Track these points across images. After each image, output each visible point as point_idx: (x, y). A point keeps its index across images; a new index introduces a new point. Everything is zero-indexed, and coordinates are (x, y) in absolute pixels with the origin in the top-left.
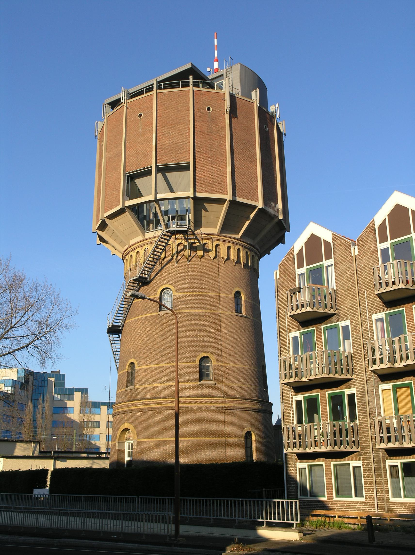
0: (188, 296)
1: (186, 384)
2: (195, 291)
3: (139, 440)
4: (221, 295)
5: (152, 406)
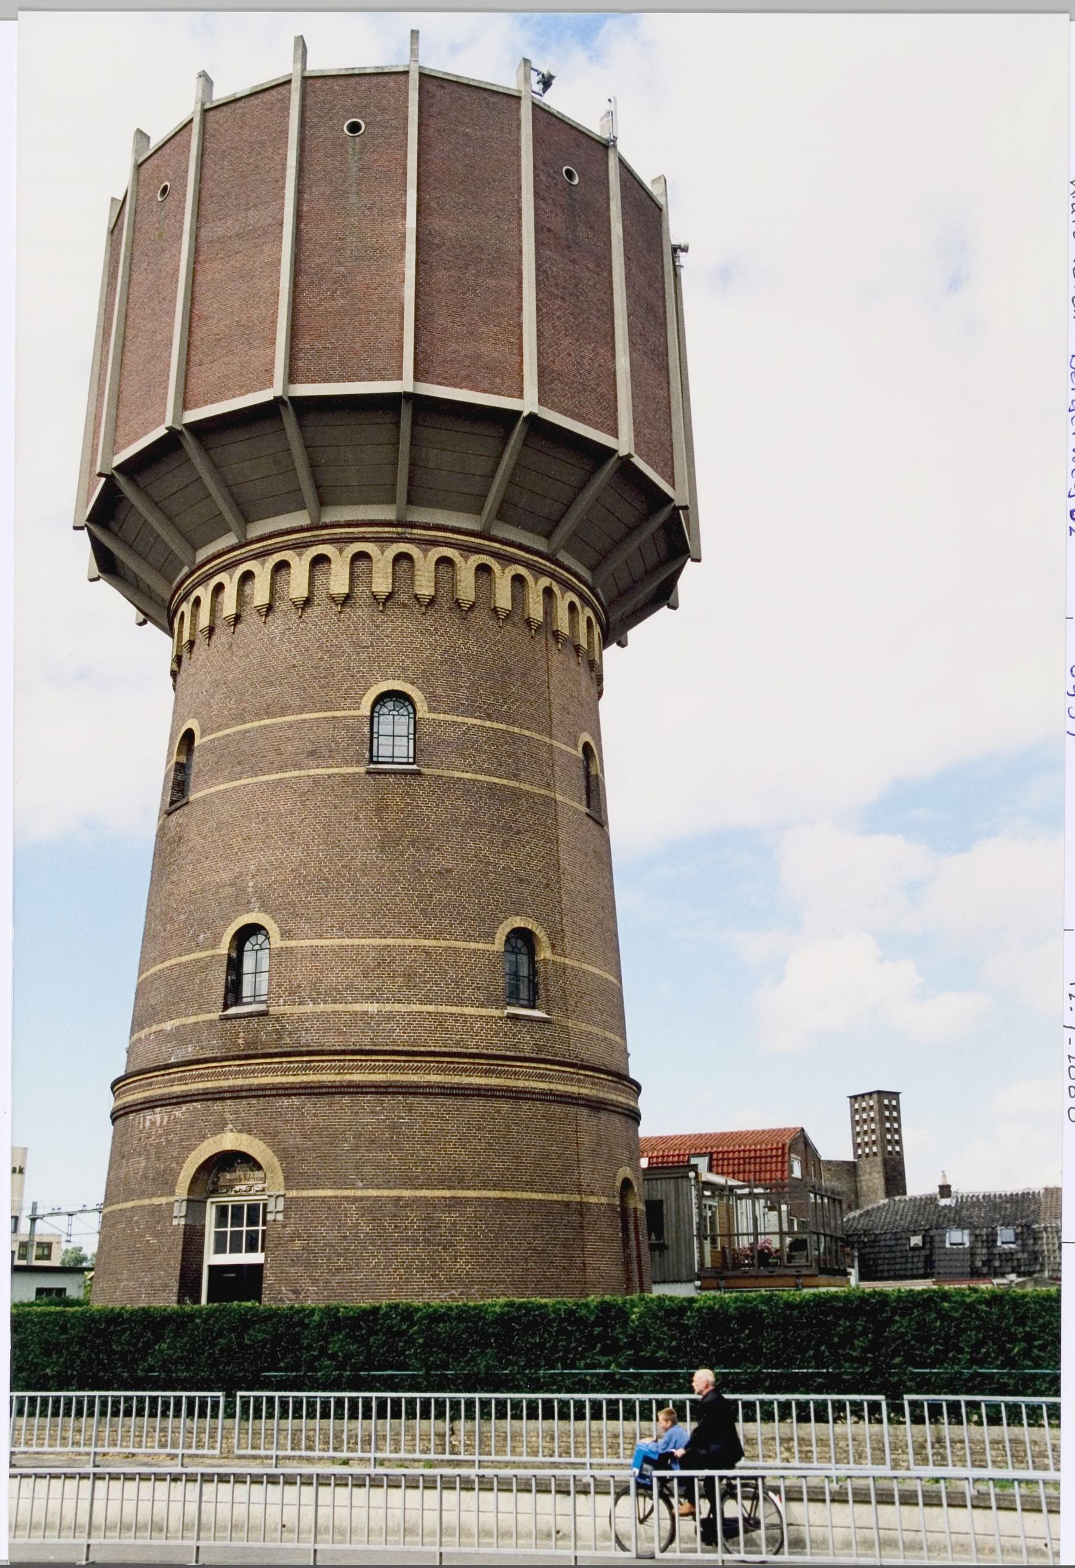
0: (468, 728)
1: (467, 1010)
2: (489, 717)
3: (293, 1193)
4: (555, 743)
5: (348, 1077)
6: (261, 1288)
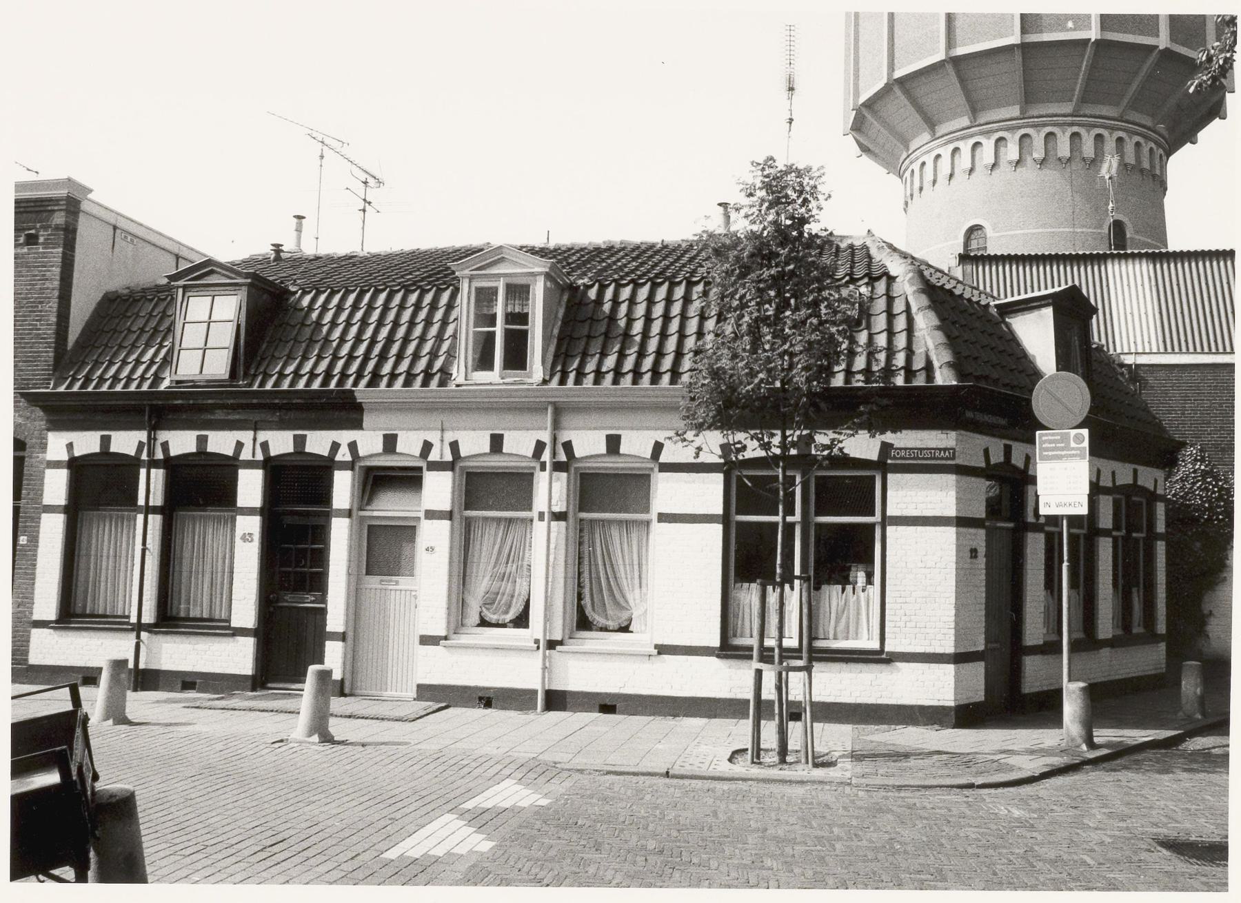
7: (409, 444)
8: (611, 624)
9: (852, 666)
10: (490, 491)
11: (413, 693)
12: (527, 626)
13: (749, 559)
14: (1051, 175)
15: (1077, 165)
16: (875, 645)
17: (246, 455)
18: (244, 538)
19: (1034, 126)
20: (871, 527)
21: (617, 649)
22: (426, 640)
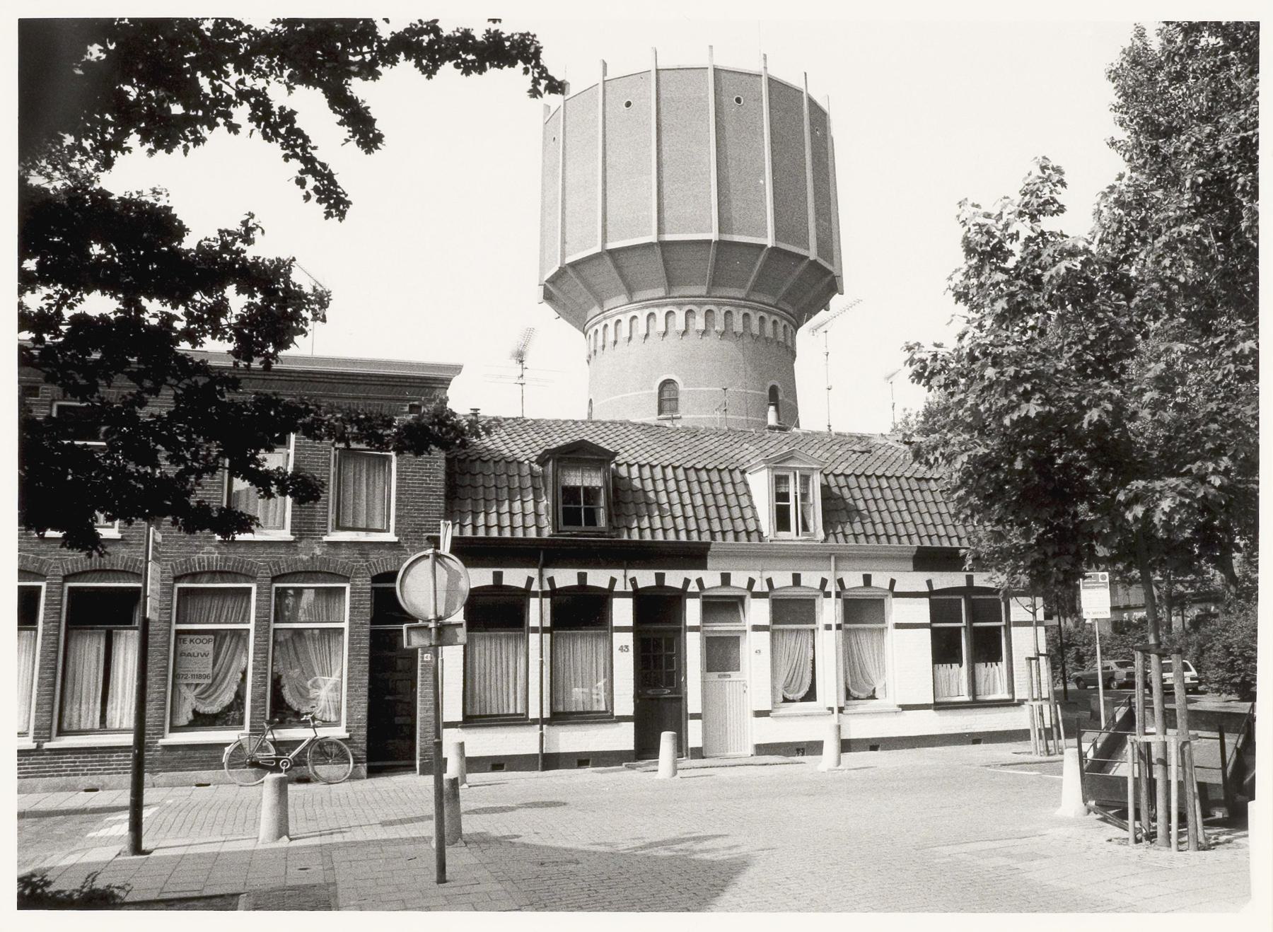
6: (370, 697)
7: (739, 580)
8: (862, 695)
9: (949, 712)
10: (792, 611)
11: (750, 750)
12: (815, 700)
13: (945, 650)
14: (729, 345)
15: (747, 340)
16: (1006, 696)
17: (619, 587)
18: (621, 649)
19: (718, 304)
20: (999, 628)
21: (873, 709)
22: (759, 714)
